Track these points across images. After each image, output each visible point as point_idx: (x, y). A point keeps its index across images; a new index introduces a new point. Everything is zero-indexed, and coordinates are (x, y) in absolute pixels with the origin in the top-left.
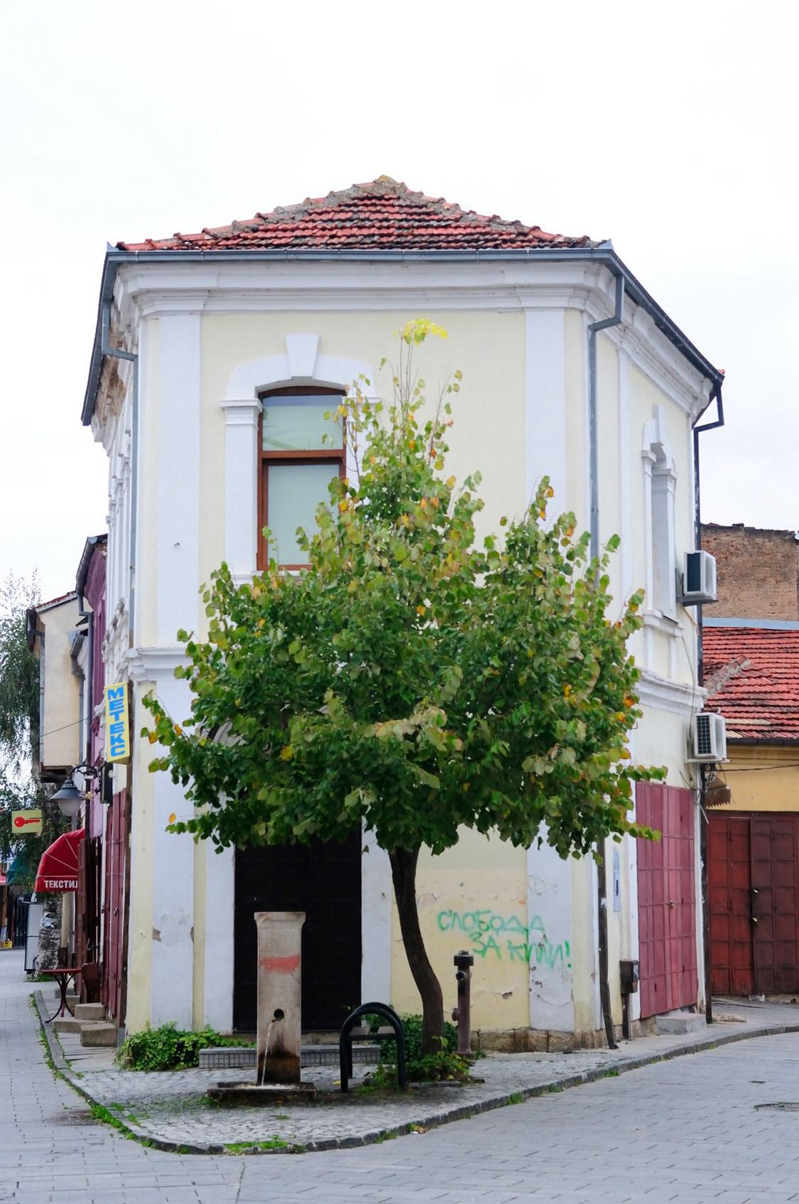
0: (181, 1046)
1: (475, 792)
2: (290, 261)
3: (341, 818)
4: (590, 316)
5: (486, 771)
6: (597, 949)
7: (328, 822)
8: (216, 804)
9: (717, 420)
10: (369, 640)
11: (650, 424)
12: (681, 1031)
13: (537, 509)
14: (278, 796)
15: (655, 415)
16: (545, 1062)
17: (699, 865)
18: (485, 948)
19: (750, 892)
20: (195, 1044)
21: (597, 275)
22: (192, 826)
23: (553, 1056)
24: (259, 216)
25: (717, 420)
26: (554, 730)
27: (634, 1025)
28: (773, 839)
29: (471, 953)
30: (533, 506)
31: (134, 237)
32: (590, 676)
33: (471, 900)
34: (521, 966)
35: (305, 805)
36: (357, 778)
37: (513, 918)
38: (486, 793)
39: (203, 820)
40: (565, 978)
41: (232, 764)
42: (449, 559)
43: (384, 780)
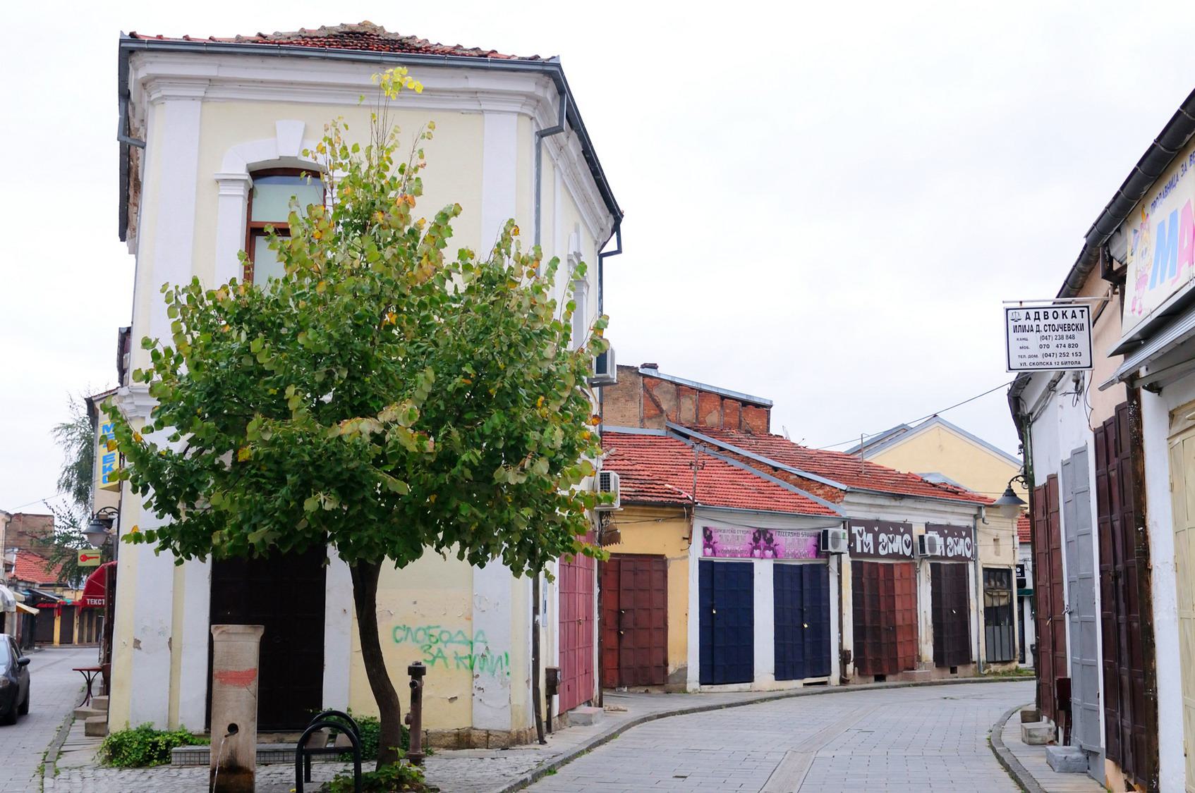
0: (155, 745)
1: (441, 505)
2: (283, 56)
3: (301, 526)
4: (538, 125)
5: (454, 480)
6: (531, 659)
7: (287, 530)
8: (176, 514)
9: (616, 248)
10: (337, 344)
11: (574, 235)
12: (588, 722)
13: (503, 246)
14: (233, 501)
15: (577, 231)
16: (488, 760)
17: (596, 590)
18: (435, 658)
19: (619, 612)
20: (168, 744)
21: (546, 87)
22: (150, 537)
23: (493, 752)
24: (260, 35)
25: (616, 248)
26: (527, 442)
27: (555, 721)
28: (635, 574)
29: (424, 664)
30: (499, 245)
31: (148, 31)
32: (564, 387)
33: (423, 616)
34: (466, 674)
35: (264, 514)
36: (320, 484)
37: (460, 632)
38: (453, 504)
39: (162, 531)
40: (505, 684)
41: (192, 473)
42: (424, 261)
43: (349, 486)
